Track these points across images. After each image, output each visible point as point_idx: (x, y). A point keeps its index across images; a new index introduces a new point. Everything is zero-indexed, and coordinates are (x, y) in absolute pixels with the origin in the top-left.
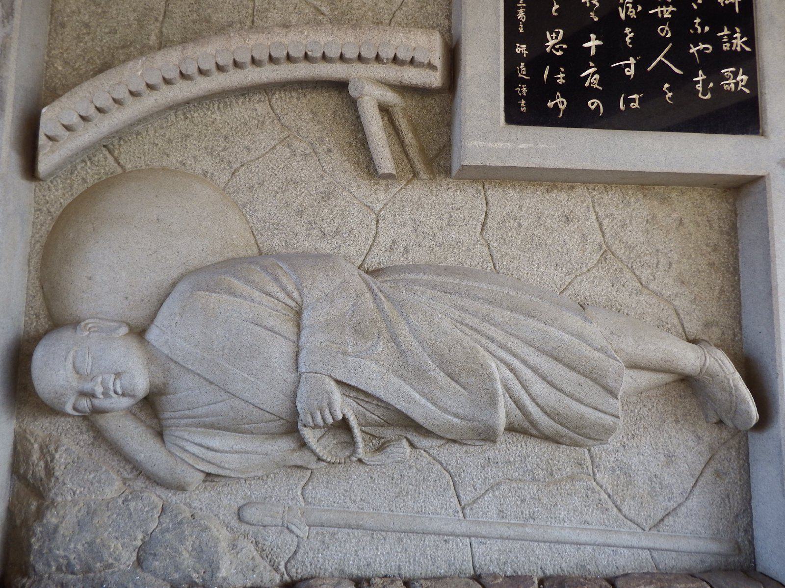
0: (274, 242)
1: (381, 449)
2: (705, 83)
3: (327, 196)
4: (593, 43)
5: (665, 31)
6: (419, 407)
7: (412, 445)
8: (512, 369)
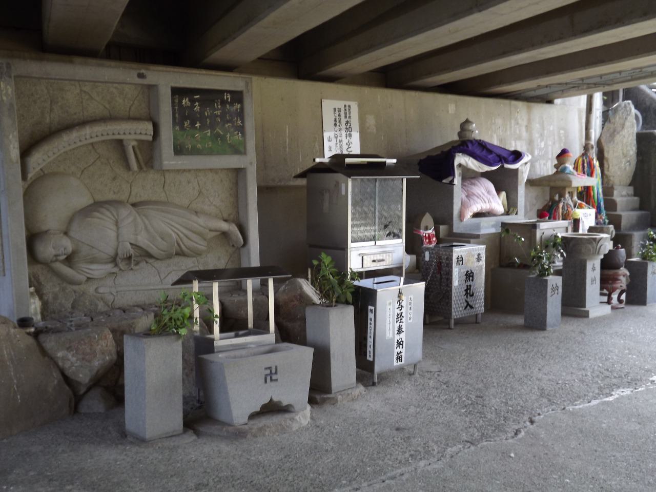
0: (99, 198)
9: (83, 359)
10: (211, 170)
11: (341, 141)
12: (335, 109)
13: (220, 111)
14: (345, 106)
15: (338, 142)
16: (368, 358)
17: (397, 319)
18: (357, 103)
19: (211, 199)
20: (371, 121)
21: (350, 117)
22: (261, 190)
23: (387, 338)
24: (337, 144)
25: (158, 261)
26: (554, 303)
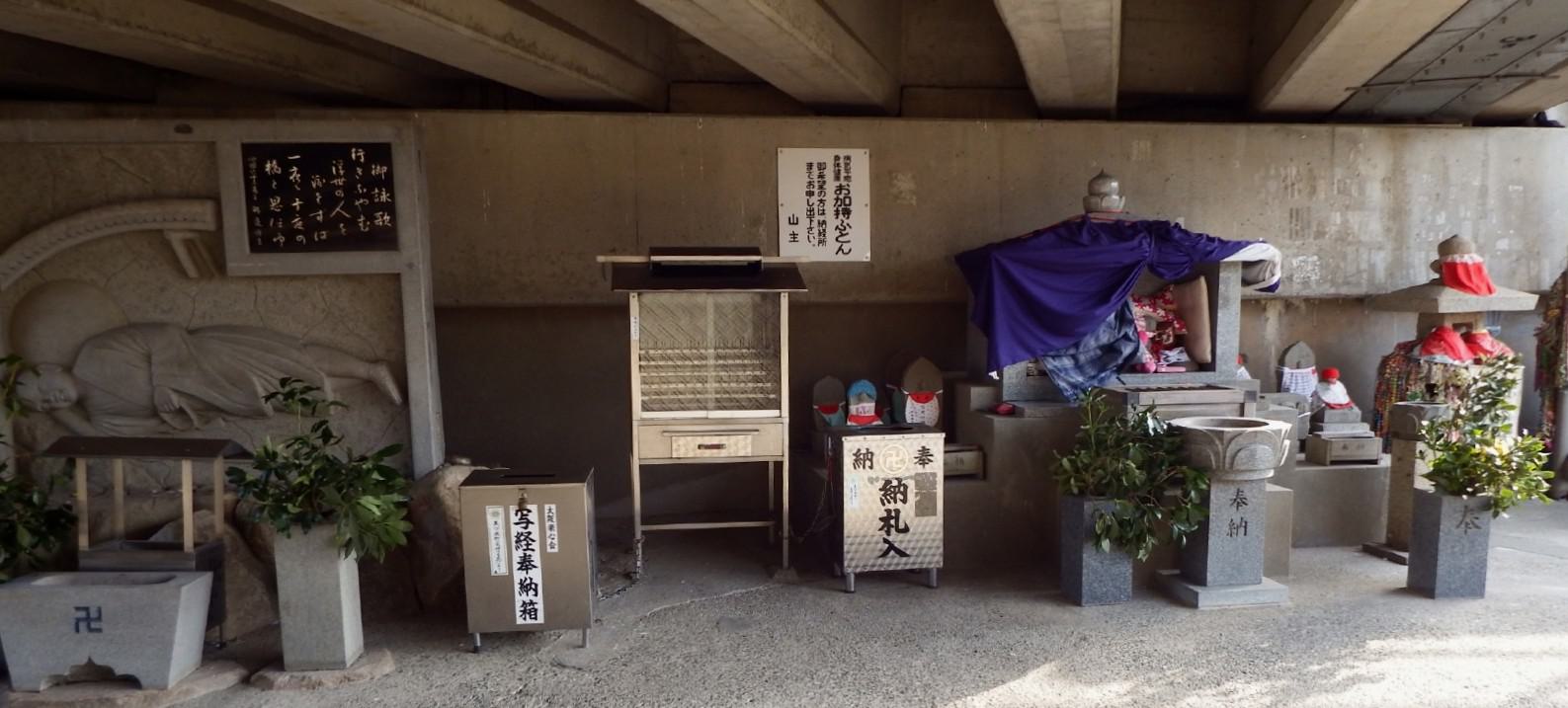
1: (207, 422)
2: (365, 222)
3: (162, 290)
4: (297, 203)
5: (339, 193)
6: (220, 400)
7: (224, 419)
8: (266, 380)
12: (810, 166)
13: (343, 179)
14: (837, 158)
15: (815, 224)
17: (517, 542)
18: (868, 151)
21: (847, 178)
22: (444, 316)
23: (493, 574)
24: (811, 228)
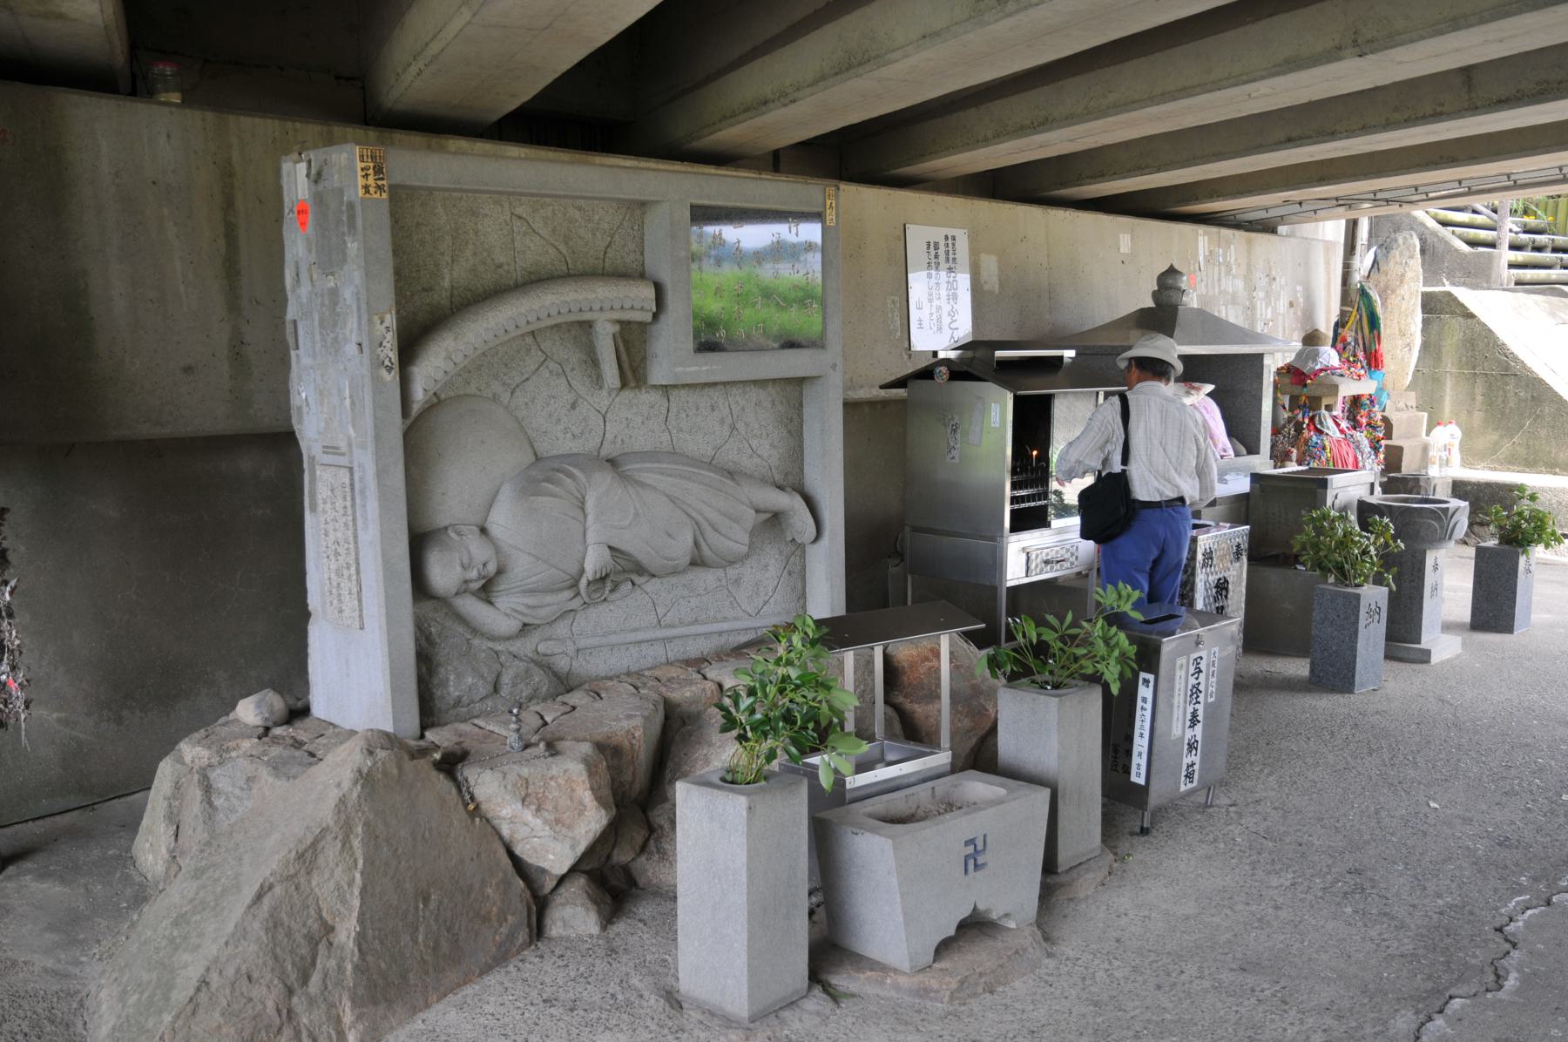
9: (558, 821)
10: (755, 382)
11: (939, 308)
16: (1134, 778)
19: (754, 443)
20: (990, 265)
25: (654, 580)
26: (1371, 635)
